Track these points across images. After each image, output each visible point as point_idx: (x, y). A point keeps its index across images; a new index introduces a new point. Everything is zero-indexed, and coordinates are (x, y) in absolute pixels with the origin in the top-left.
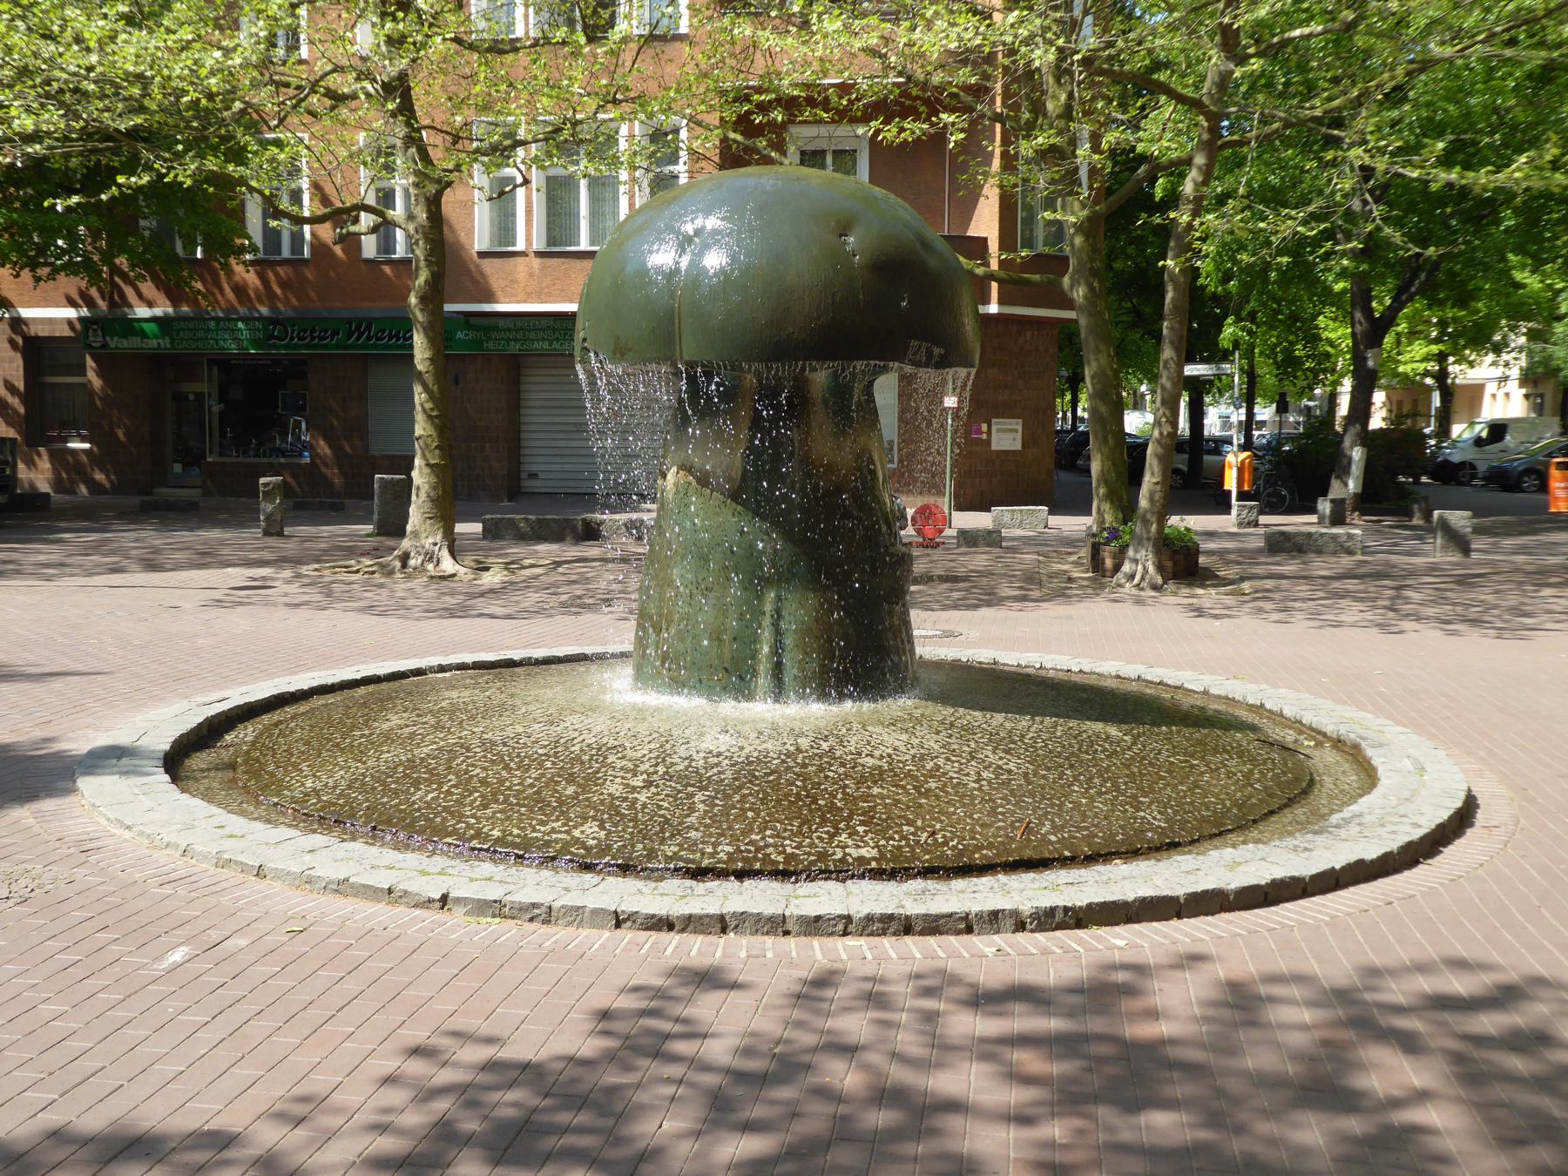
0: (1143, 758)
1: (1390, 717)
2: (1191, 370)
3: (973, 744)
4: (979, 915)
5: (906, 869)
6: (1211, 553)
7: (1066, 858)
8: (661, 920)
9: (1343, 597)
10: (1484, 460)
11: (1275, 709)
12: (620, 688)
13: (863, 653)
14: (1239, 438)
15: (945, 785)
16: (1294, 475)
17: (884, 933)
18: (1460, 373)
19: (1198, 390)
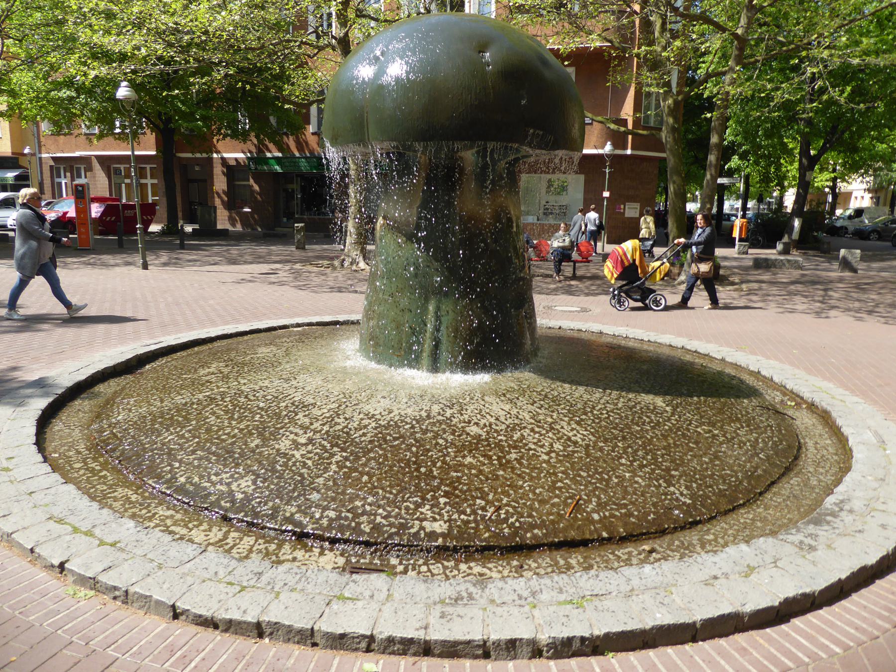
0: (678, 429)
1: (847, 388)
2: (720, 181)
3: (555, 415)
4: (497, 644)
5: (466, 547)
6: (725, 267)
7: (604, 539)
8: (206, 619)
9: (796, 295)
10: (851, 226)
11: (767, 376)
12: (350, 353)
13: (497, 335)
14: (740, 214)
15: (522, 457)
16: (767, 230)
17: (404, 653)
18: (842, 186)
19: (722, 190)
